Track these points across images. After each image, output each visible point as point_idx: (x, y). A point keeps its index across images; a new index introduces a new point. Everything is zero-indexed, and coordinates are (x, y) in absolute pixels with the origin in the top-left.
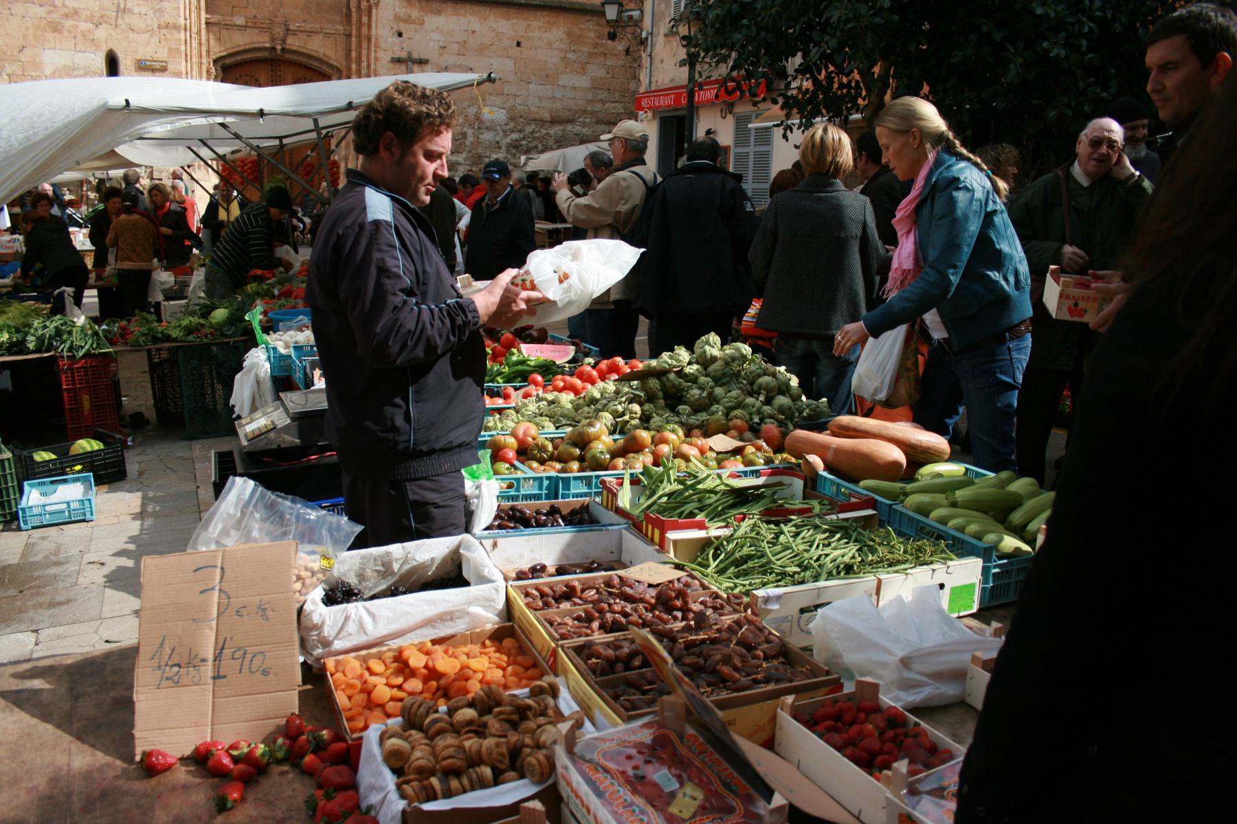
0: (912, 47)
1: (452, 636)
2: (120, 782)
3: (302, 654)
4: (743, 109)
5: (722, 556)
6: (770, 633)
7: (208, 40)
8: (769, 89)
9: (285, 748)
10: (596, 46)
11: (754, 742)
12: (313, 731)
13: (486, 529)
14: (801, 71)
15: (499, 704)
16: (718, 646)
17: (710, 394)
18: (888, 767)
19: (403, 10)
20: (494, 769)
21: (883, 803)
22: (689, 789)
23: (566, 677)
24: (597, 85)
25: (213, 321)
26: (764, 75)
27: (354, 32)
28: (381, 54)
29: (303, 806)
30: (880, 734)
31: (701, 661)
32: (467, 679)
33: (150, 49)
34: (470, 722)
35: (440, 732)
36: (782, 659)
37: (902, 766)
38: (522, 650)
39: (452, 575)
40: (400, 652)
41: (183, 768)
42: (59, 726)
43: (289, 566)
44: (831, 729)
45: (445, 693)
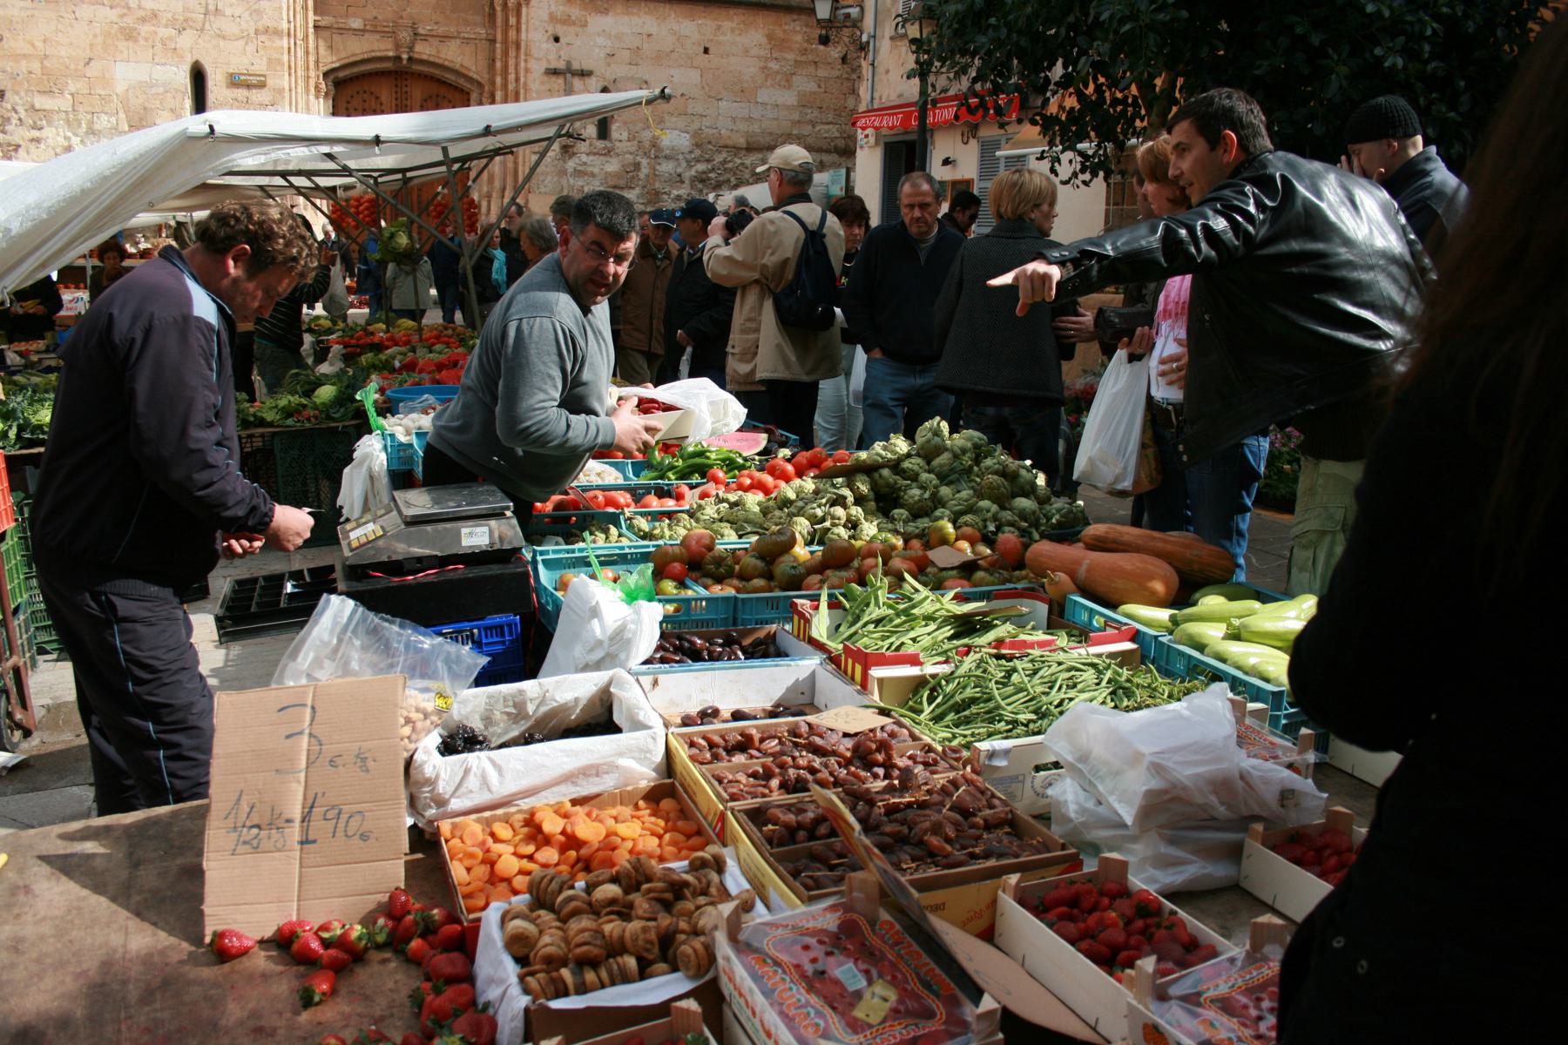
0: (1204, 52)
1: (598, 796)
2: (187, 968)
3: (412, 815)
4: (989, 132)
5: (939, 700)
6: (993, 796)
7: (317, 48)
8: (1024, 106)
9: (387, 930)
10: (804, 52)
11: (970, 933)
12: (423, 910)
13: (645, 663)
14: (1066, 82)
15: (649, 879)
16: (927, 812)
17: (934, 495)
18: (1132, 966)
19: (560, 10)
20: (640, 960)
21: (1125, 1011)
22: (880, 988)
23: (736, 848)
24: (804, 103)
25: (318, 401)
26: (1017, 88)
27: (499, 37)
28: (533, 64)
29: (407, 1002)
30: (1126, 924)
31: (900, 832)
32: (614, 849)
33: (243, 59)
34: (613, 901)
35: (575, 913)
36: (1008, 829)
37: (1148, 964)
38: (684, 813)
39: (599, 719)
40: (532, 814)
41: (263, 953)
42: (114, 899)
43: (396, 705)
44: (1062, 917)
45: (586, 865)
